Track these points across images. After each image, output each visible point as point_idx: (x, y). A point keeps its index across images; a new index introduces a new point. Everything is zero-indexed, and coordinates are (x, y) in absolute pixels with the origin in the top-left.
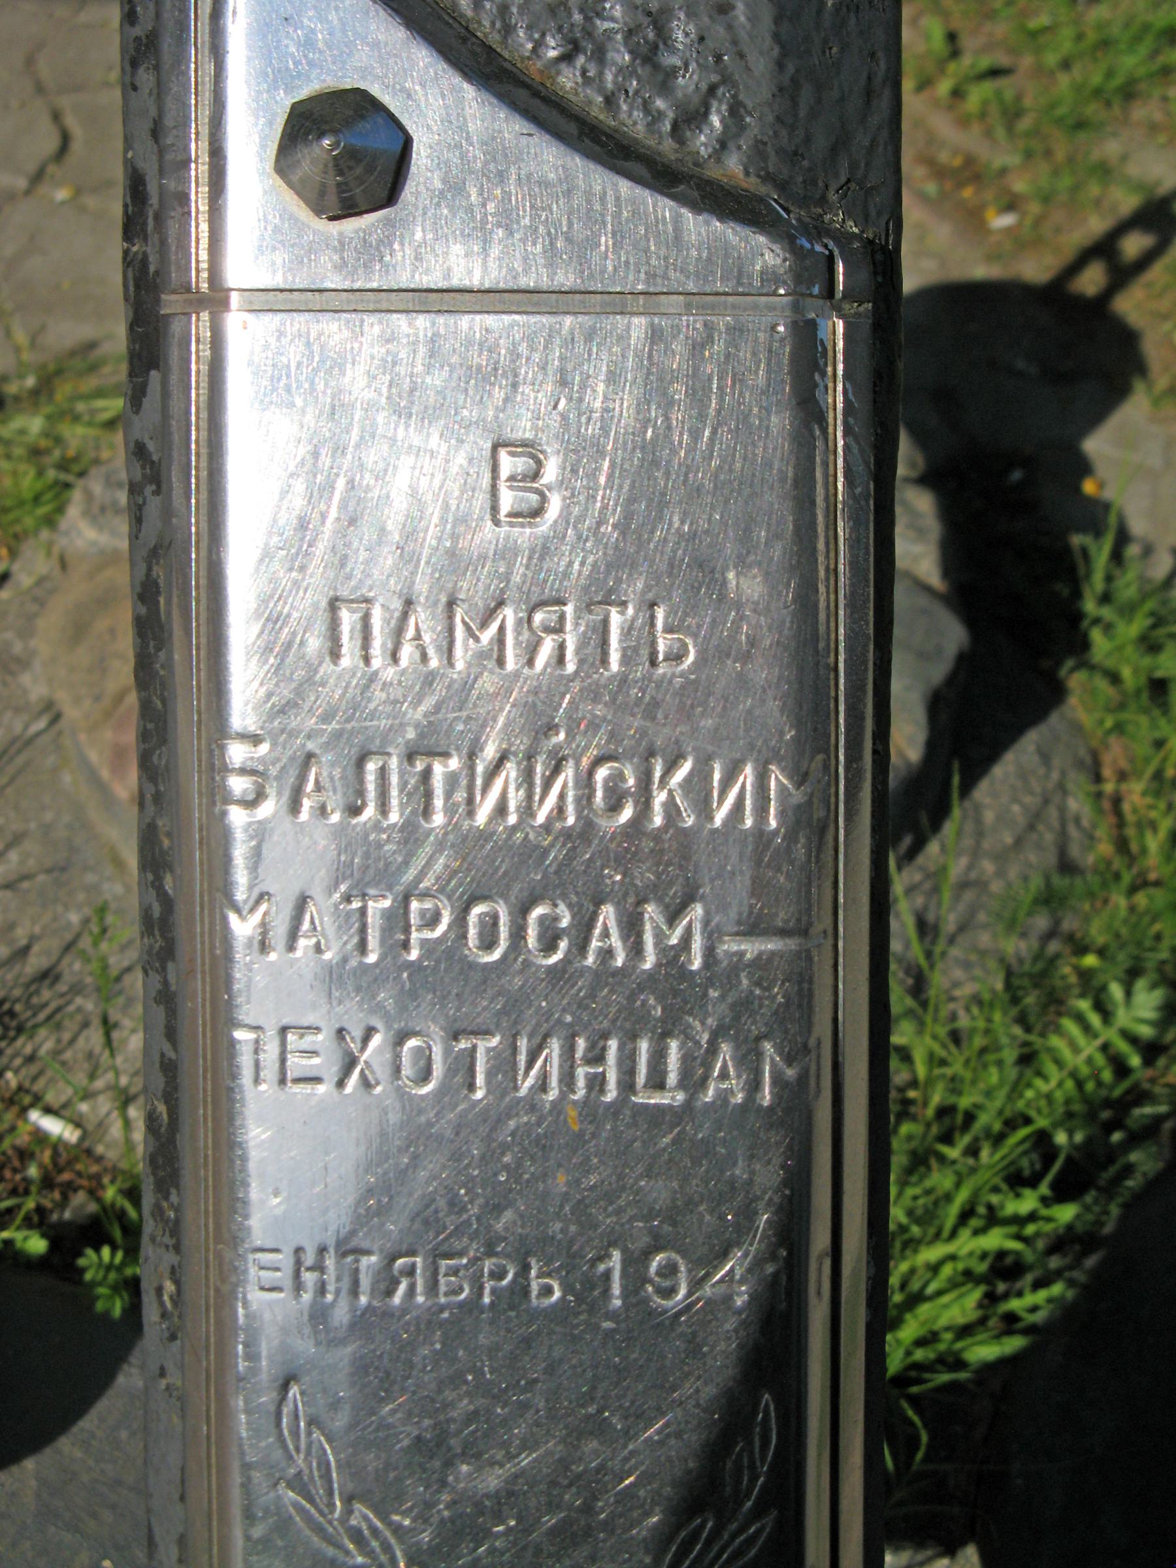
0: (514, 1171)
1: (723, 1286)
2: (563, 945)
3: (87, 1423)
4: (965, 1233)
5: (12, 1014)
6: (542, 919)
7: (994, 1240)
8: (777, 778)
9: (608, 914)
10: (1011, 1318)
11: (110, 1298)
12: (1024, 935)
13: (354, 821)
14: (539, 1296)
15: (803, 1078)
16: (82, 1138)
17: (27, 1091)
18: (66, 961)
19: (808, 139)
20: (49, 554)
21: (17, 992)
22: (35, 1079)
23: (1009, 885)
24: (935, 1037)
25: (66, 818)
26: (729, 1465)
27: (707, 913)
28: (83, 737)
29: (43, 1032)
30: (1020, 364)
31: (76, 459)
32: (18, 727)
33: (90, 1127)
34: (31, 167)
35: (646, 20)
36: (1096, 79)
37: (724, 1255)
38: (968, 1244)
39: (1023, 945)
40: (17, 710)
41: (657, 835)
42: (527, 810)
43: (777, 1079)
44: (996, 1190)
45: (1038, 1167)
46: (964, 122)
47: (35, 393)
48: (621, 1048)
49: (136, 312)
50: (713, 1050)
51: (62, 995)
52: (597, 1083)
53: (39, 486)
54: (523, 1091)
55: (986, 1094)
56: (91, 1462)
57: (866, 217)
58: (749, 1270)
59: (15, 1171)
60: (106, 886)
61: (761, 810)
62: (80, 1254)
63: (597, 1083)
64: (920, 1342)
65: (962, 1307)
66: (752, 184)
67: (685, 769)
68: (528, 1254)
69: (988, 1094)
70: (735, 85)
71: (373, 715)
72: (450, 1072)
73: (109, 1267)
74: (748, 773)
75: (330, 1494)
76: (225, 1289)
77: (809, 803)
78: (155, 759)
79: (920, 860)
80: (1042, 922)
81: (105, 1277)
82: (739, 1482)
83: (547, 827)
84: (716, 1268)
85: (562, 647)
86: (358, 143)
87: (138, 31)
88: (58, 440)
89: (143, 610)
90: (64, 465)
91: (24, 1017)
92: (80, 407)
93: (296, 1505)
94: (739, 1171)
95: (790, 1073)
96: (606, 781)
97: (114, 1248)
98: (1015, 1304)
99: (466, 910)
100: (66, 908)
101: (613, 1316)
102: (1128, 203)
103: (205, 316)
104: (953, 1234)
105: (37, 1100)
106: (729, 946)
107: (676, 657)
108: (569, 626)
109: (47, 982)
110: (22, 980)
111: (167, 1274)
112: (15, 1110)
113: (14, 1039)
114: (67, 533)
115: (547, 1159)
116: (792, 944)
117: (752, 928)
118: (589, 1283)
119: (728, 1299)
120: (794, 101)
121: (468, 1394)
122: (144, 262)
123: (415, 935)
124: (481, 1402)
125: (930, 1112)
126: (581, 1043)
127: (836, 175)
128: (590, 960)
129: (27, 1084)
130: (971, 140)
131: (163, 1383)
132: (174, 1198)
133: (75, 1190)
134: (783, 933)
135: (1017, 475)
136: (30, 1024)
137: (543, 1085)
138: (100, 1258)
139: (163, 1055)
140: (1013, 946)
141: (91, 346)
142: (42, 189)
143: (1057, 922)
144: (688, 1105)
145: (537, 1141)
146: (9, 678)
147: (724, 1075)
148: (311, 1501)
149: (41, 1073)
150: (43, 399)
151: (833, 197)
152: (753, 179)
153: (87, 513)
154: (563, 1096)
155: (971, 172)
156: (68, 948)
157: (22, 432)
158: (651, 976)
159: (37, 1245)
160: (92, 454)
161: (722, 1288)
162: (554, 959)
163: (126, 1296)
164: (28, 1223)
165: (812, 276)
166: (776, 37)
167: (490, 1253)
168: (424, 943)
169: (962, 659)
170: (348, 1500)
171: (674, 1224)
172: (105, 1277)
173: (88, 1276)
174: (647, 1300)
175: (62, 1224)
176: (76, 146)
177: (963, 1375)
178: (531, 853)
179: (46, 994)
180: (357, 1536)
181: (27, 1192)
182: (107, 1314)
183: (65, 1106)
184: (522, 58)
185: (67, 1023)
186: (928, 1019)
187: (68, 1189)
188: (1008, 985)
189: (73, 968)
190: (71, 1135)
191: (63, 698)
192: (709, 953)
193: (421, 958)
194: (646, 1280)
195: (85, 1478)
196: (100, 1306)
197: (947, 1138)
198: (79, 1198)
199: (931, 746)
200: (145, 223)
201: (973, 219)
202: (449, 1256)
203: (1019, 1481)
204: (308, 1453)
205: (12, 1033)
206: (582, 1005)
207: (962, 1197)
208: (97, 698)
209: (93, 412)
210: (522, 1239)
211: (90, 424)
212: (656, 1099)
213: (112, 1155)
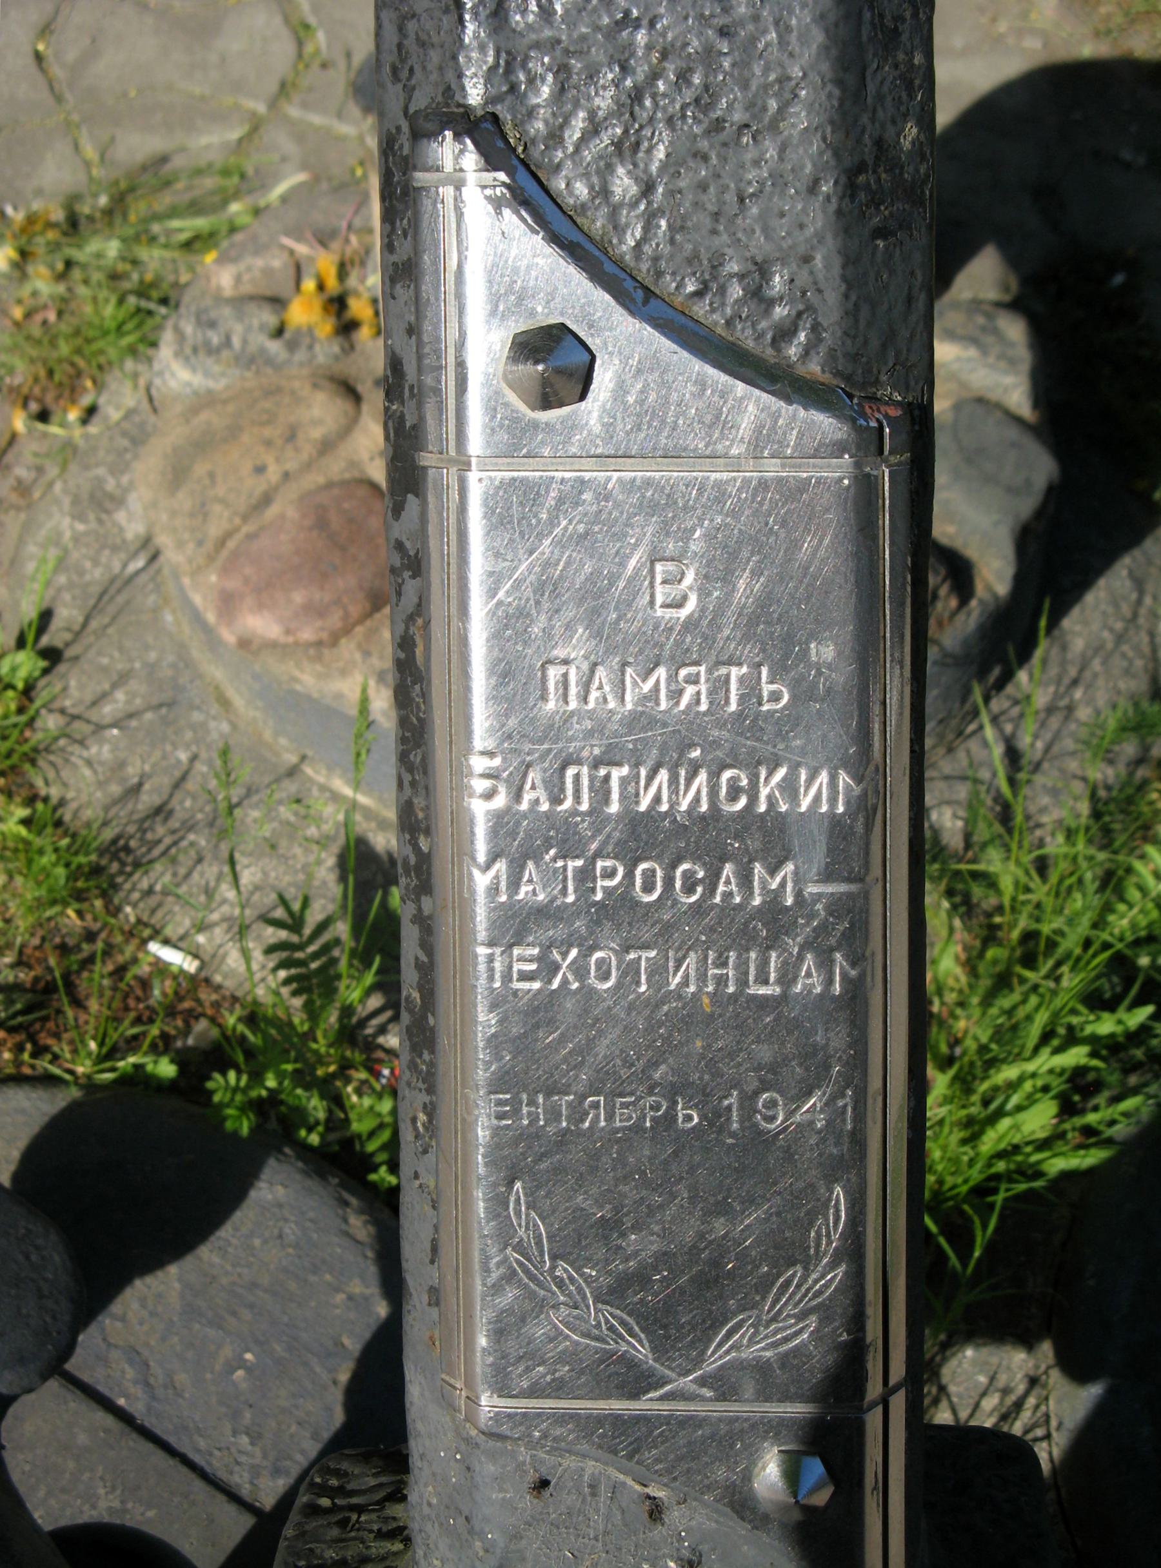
0: (667, 1040)
1: (808, 1116)
2: (699, 889)
3: (225, 1232)
4: (1046, 1052)
5: (127, 849)
6: (685, 872)
7: (1076, 1056)
8: (844, 778)
9: (728, 869)
10: (1088, 1131)
11: (239, 1118)
12: (1111, 762)
13: (559, 808)
14: (684, 1121)
15: (862, 976)
16: (201, 969)
17: (146, 925)
18: (178, 796)
19: (866, 343)
20: (136, 386)
22: (153, 911)
23: (1098, 713)
24: (1018, 863)
25: (171, 658)
26: (813, 1234)
27: (796, 867)
28: (186, 581)
29: (158, 867)
30: (1126, 155)
31: (154, 285)
32: (116, 566)
33: (207, 958)
35: (754, 268)
37: (809, 1094)
38: (1046, 1061)
39: (1110, 772)
40: (115, 549)
41: (762, 816)
42: (673, 805)
43: (844, 975)
44: (1073, 1012)
45: (1118, 989)
47: (109, 213)
48: (739, 957)
49: (395, 451)
50: (801, 958)
51: (173, 832)
52: (721, 981)
53: (122, 314)
54: (672, 987)
55: (1071, 921)
56: (229, 1268)
57: (907, 387)
58: (826, 1104)
59: (138, 999)
60: (212, 724)
61: (833, 800)
62: (209, 1078)
63: (721, 981)
64: (1001, 1155)
65: (1039, 1119)
66: (827, 378)
67: (782, 772)
68: (676, 1094)
69: (1071, 922)
70: (815, 311)
71: (571, 740)
72: (622, 976)
73: (236, 1089)
74: (824, 777)
75: (542, 1254)
76: (469, 1119)
77: (865, 794)
78: (412, 757)
79: (1010, 689)
80: (1130, 749)
81: (232, 1099)
82: (818, 1245)
83: (689, 812)
84: (804, 1103)
85: (698, 693)
86: (558, 363)
87: (394, 258)
88: (135, 262)
89: (402, 656)
90: (142, 292)
91: (139, 853)
92: (156, 228)
93: (517, 1261)
94: (819, 1038)
95: (853, 973)
96: (728, 780)
97: (239, 1072)
98: (1092, 1118)
99: (635, 866)
100: (175, 746)
101: (733, 1135)
103: (453, 470)
104: (1036, 1050)
105: (156, 934)
106: (812, 889)
107: (775, 697)
108: (703, 679)
109: (158, 819)
110: (136, 817)
111: (420, 1107)
112: (135, 942)
113: (130, 875)
114: (160, 374)
115: (688, 1031)
116: (853, 888)
117: (827, 876)
118: (717, 1114)
119: (812, 1123)
120: (857, 321)
121: (636, 1187)
122: (402, 417)
123: (600, 883)
124: (644, 1193)
125: (1015, 934)
126: (711, 955)
127: (886, 364)
128: (718, 899)
129: (145, 918)
131: (417, 1183)
132: (426, 1056)
133: (197, 1018)
134: (849, 880)
135: (1119, 279)
136: (144, 860)
137: (685, 982)
138: (227, 1081)
139: (417, 958)
140: (1098, 772)
141: (164, 159)
143: (1146, 749)
144: (784, 996)
145: (682, 1019)
146: (104, 516)
147: (809, 975)
148: (529, 1260)
149: (160, 905)
150: (118, 220)
151: (884, 378)
152: (827, 375)
153: (178, 354)
154: (700, 989)
156: (177, 785)
157: (99, 255)
158: (759, 910)
159: (166, 1069)
160: (171, 278)
161: (808, 1116)
162: (693, 899)
163: (252, 1116)
164: (154, 1049)
165: (869, 444)
166: (844, 278)
167: (651, 1092)
168: (604, 888)
169: (1051, 490)
170: (554, 1258)
171: (775, 1074)
172: (232, 1099)
173: (217, 1098)
174: (756, 1125)
175: (187, 1049)
177: (1038, 1184)
178: (680, 830)
179: (160, 830)
180: (560, 1284)
181: (151, 1021)
182: (235, 1134)
183: (182, 938)
184: (669, 294)
185: (181, 857)
186: (1014, 846)
187: (191, 1016)
188: (1096, 815)
189: (184, 805)
190: (190, 966)
191: (163, 540)
192: (799, 895)
193: (603, 899)
194: (756, 1111)
195: (224, 1281)
196: (229, 1125)
197: (1029, 961)
198: (201, 1025)
199: (1019, 580)
200: (402, 392)
202: (621, 1095)
203: (1091, 1283)
204: (527, 1228)
205: (128, 869)
206: (712, 930)
207: (1041, 1019)
208: (200, 543)
209: (169, 233)
210: (673, 1085)
211: (166, 246)
212: (763, 991)
213: (229, 984)
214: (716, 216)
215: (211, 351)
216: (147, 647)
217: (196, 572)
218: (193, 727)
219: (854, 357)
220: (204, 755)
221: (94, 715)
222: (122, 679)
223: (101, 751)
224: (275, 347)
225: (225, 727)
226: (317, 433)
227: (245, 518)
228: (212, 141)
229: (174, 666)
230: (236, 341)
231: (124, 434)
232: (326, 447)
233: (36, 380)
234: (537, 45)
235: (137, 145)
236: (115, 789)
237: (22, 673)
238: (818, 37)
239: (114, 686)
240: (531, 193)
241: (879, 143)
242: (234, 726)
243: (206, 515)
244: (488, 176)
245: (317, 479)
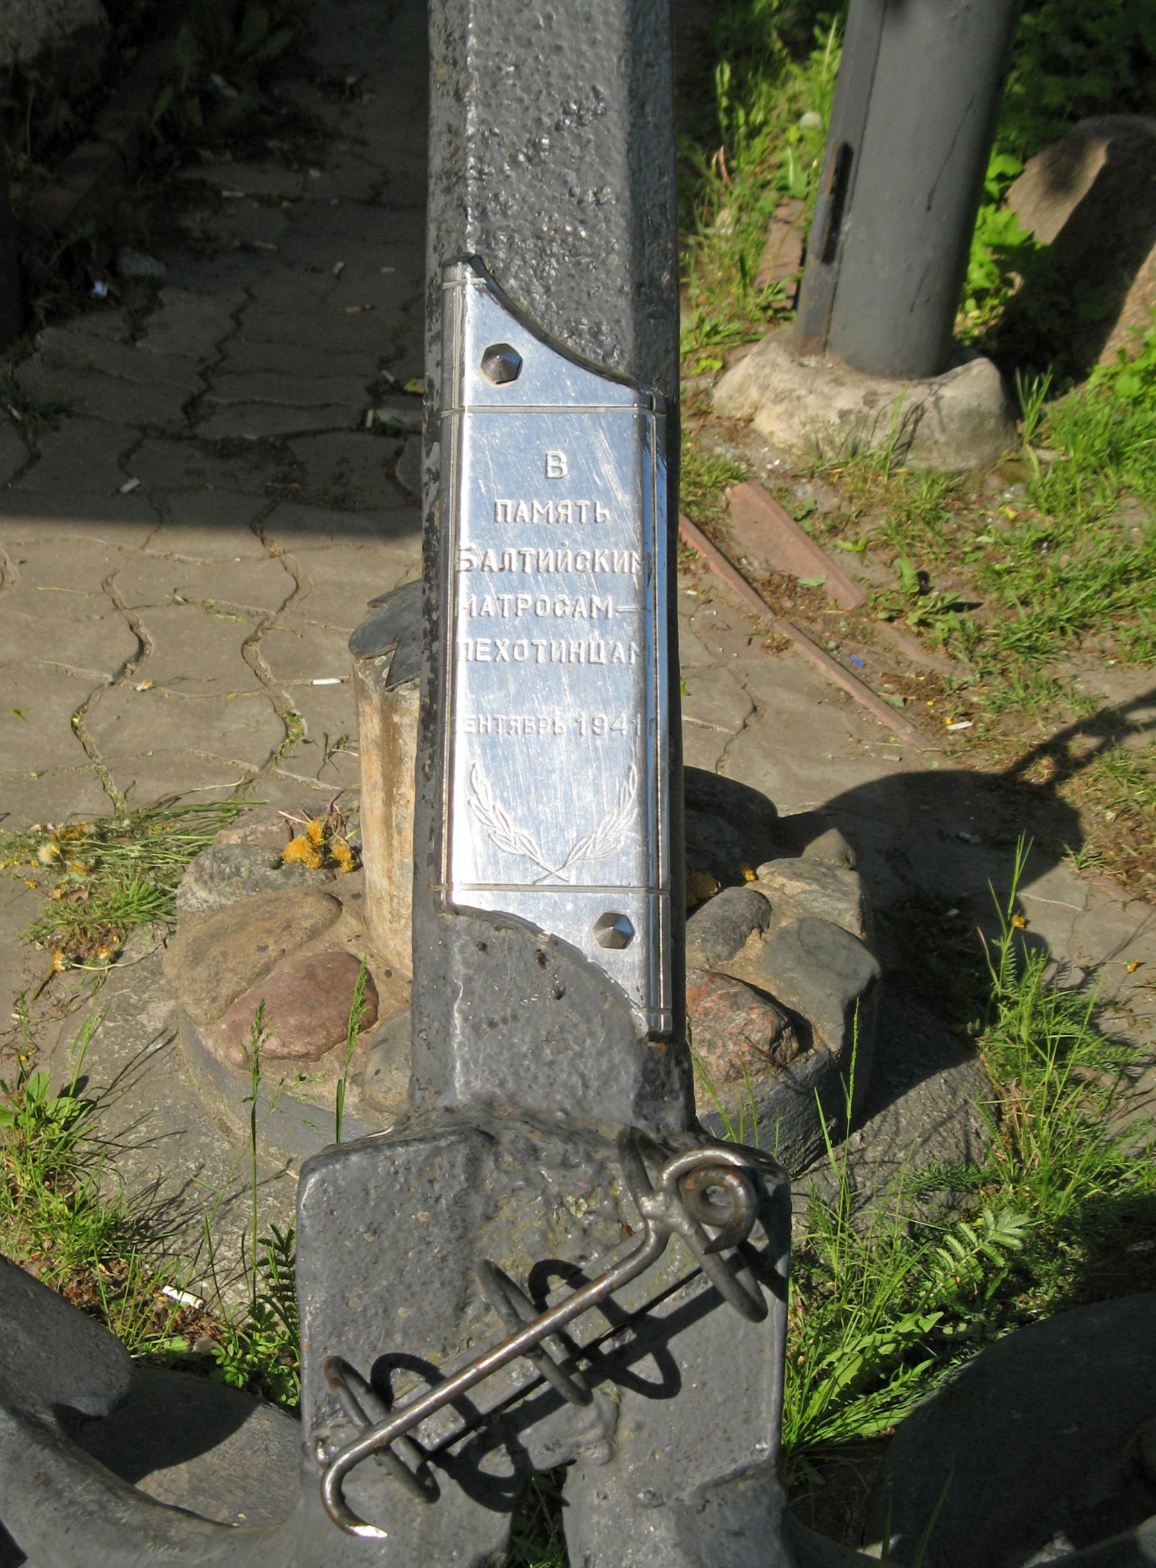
3: (223, 1446)
5: (147, 1227)
18: (188, 1191)
21: (150, 1213)
34: (116, 665)
36: (1052, 611)
46: (930, 648)
102: (1074, 714)
105: (168, 1281)
130: (936, 662)
135: (954, 912)
142: (124, 683)
155: (933, 687)
165: (646, 403)
173: (219, 1362)
176: (151, 650)
182: (232, 1385)
189: (192, 1197)
201: (935, 723)
208: (214, 1000)
214: (578, 303)
215: (224, 877)
216: (165, 1097)
217: (212, 1021)
218: (201, 1147)
219: (640, 367)
220: (209, 1164)
221: (121, 1141)
222: (143, 1119)
223: (128, 1164)
224: (274, 874)
225: (227, 1146)
226: (307, 924)
227: (250, 982)
228: (214, 789)
229: (186, 1108)
230: (244, 871)
231: (144, 969)
232: (314, 934)
233: (73, 936)
234: (500, 228)
235: (152, 789)
236: (138, 1188)
237: (65, 1112)
238: (623, 223)
239: (138, 1122)
240: (494, 288)
241: (651, 276)
242: (233, 1146)
243: (219, 981)
244: (477, 280)
245: (305, 954)
